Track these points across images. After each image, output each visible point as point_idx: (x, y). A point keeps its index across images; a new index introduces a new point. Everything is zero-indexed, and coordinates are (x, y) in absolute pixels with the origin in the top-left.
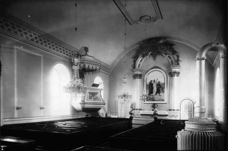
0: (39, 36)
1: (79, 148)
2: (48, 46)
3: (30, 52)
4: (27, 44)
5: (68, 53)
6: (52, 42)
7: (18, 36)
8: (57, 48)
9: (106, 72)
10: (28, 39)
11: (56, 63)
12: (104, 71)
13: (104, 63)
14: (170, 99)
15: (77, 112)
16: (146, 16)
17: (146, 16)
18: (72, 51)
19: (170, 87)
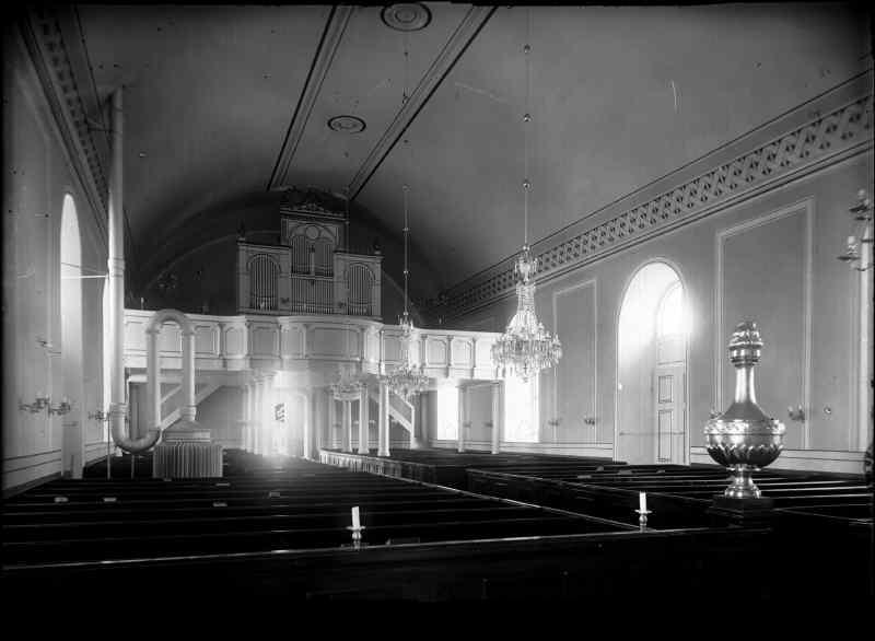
0: (814, 124)
1: (602, 534)
2: (775, 166)
3: (768, 217)
4: (797, 181)
5: (628, 225)
6: (668, 195)
7: (762, 181)
8: (696, 192)
9: (553, 270)
10: (790, 165)
11: (653, 257)
12: (572, 263)
13: (836, 88)
14: (491, 464)
15: (225, 329)
16: (426, 26)
17: (426, 26)
18: (644, 206)
19: (368, 173)
